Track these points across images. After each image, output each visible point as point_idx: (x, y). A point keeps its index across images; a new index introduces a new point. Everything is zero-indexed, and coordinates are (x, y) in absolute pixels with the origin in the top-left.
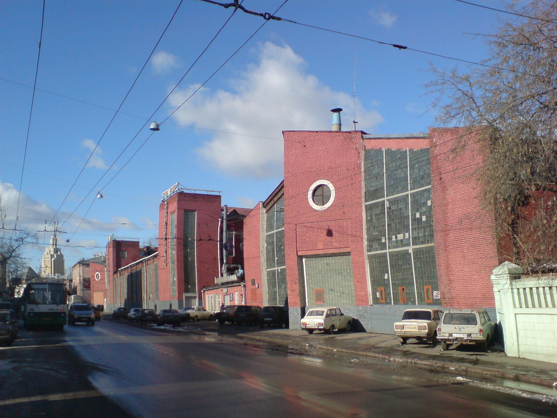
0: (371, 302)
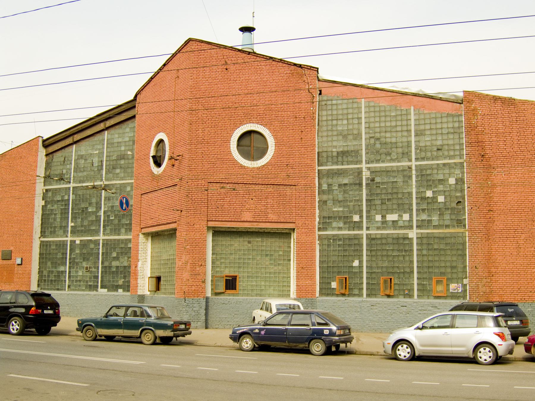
0: (317, 294)
